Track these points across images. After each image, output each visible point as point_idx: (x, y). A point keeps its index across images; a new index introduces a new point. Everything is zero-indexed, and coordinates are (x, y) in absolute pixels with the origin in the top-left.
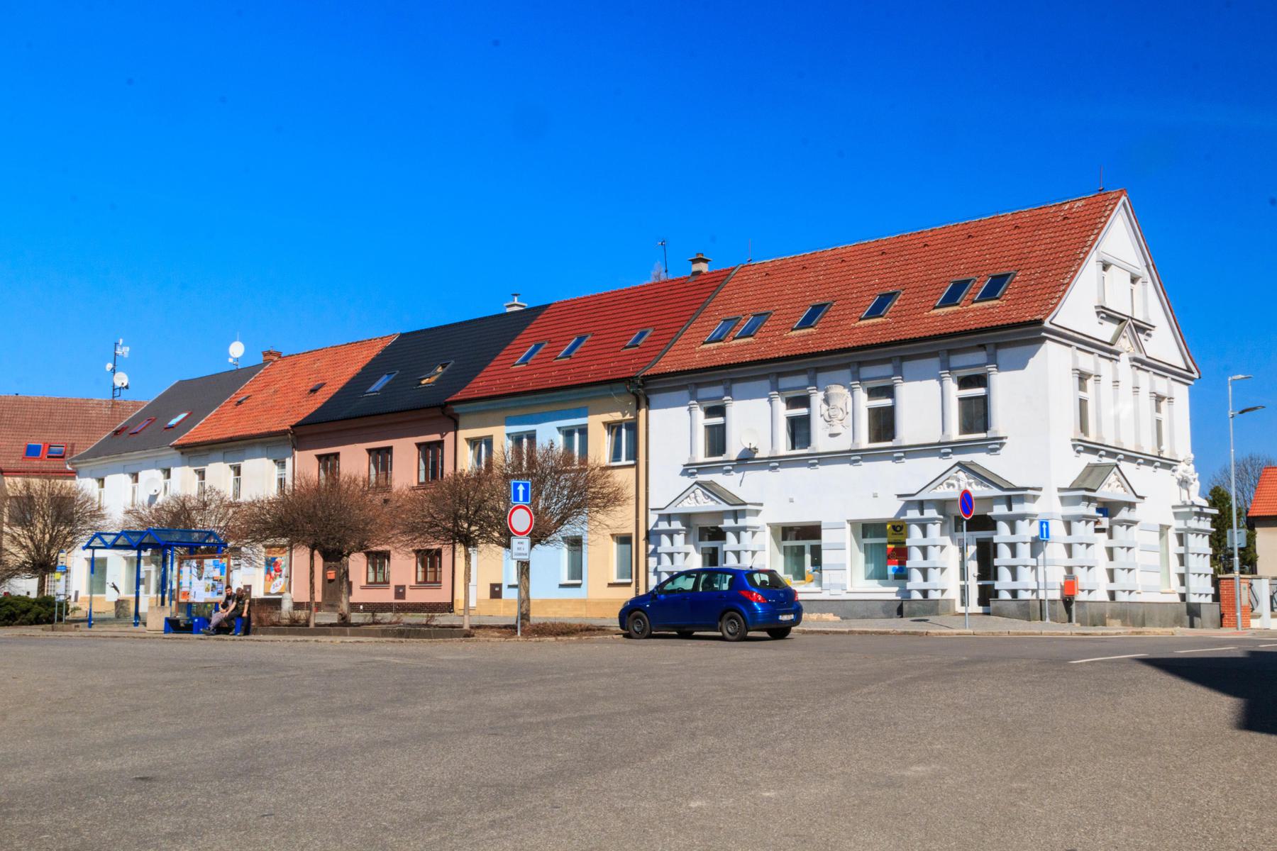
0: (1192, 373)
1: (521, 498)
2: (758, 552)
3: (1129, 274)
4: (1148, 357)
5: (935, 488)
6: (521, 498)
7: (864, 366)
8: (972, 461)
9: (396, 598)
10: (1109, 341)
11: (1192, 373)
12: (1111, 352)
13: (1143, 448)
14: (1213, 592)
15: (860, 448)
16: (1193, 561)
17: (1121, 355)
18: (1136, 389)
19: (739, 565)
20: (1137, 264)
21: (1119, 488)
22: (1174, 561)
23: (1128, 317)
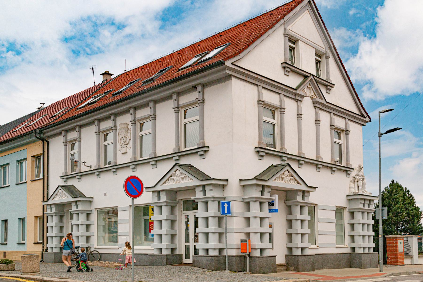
0: (365, 118)
1: (226, 212)
2: (92, 236)
3: (314, 51)
4: (327, 102)
5: (165, 183)
6: (226, 212)
7: (157, 104)
8: (190, 164)
9: (374, 252)
10: (295, 88)
11: (365, 118)
12: (296, 94)
13: (322, 158)
14: (374, 246)
15: (137, 160)
16: (359, 229)
17: (305, 98)
18: (317, 122)
19: (88, 244)
20: (322, 45)
21: (291, 181)
22: (347, 228)
23: (311, 74)
